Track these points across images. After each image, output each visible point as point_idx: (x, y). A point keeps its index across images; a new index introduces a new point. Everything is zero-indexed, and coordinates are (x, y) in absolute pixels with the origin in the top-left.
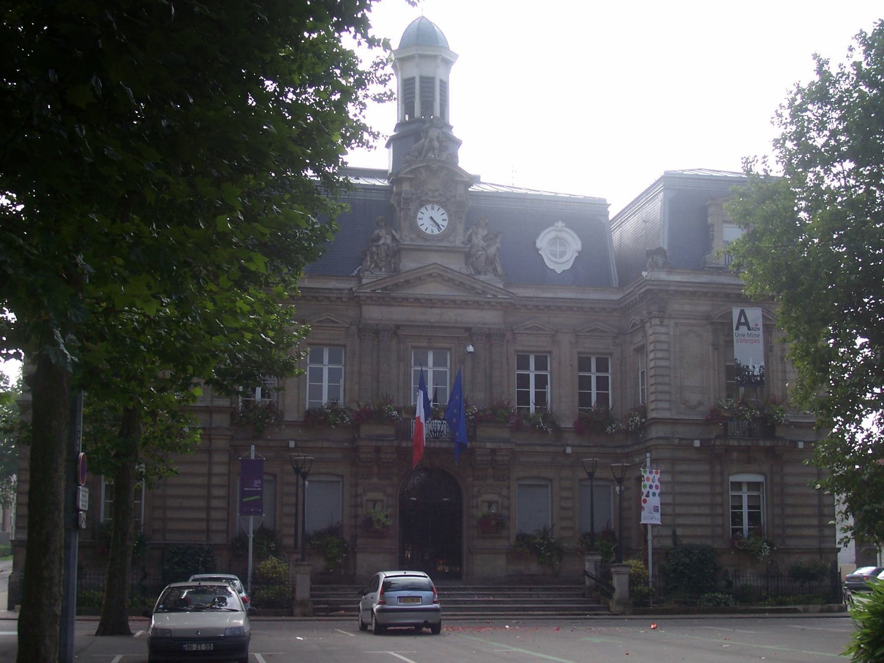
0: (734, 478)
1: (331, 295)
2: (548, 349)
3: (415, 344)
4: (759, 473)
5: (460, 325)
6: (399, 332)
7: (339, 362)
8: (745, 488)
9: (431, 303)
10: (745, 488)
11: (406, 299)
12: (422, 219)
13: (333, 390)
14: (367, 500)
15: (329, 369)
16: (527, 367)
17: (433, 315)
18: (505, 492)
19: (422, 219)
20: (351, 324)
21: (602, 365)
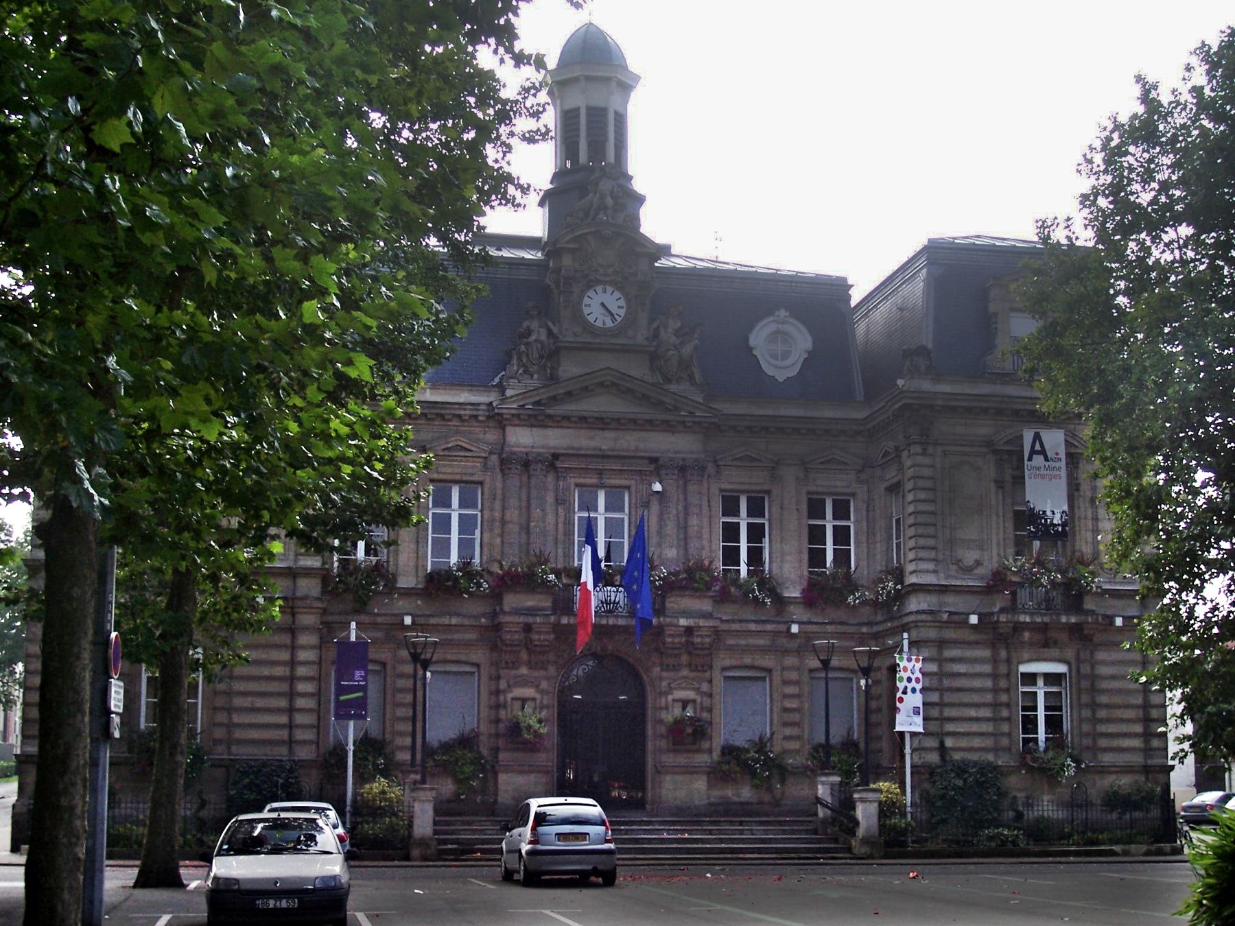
0: (1023, 668)
1: (462, 412)
2: (766, 488)
6: (559, 464)
7: (474, 506)
8: (1040, 682)
10: (1040, 682)
12: (589, 306)
14: (513, 699)
16: (736, 513)
18: (705, 687)
19: (589, 306)
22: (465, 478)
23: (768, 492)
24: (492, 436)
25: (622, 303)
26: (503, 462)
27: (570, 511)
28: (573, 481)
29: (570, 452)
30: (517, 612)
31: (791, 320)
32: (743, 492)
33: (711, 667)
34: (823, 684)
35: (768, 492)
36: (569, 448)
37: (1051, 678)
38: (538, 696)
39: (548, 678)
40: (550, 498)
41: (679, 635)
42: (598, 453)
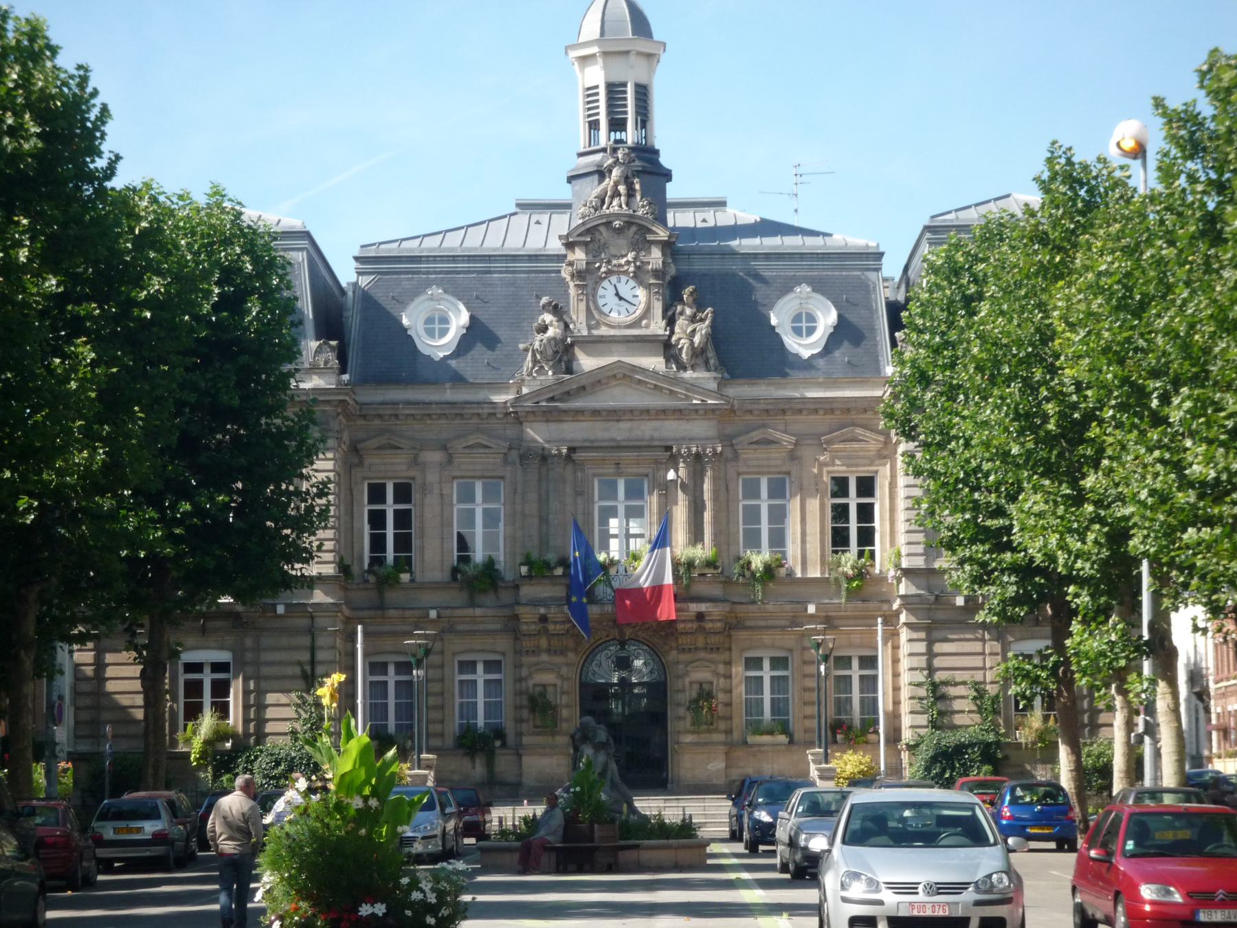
0: (188, 657)
1: (480, 411)
2: (784, 469)
3: (595, 471)
4: (222, 648)
5: (657, 443)
6: (575, 456)
7: (497, 500)
8: (207, 670)
9: (615, 415)
10: (207, 670)
11: (580, 412)
12: (604, 297)
13: (489, 540)
14: (691, 683)
15: (484, 510)
16: (383, 500)
17: (621, 431)
18: (721, 668)
19: (604, 297)
20: (510, 449)
21: (403, 493)
22: (486, 474)
23: (789, 473)
24: (511, 432)
25: (601, 292)
26: (522, 457)
27: (591, 501)
28: (590, 472)
29: (631, 444)
30: (536, 603)
31: (446, 296)
32: (763, 474)
33: (730, 649)
34: (980, 664)
35: (789, 473)
36: (585, 441)
37: (218, 667)
38: (559, 682)
39: (568, 665)
40: (569, 490)
41: (691, 621)
42: (613, 444)
